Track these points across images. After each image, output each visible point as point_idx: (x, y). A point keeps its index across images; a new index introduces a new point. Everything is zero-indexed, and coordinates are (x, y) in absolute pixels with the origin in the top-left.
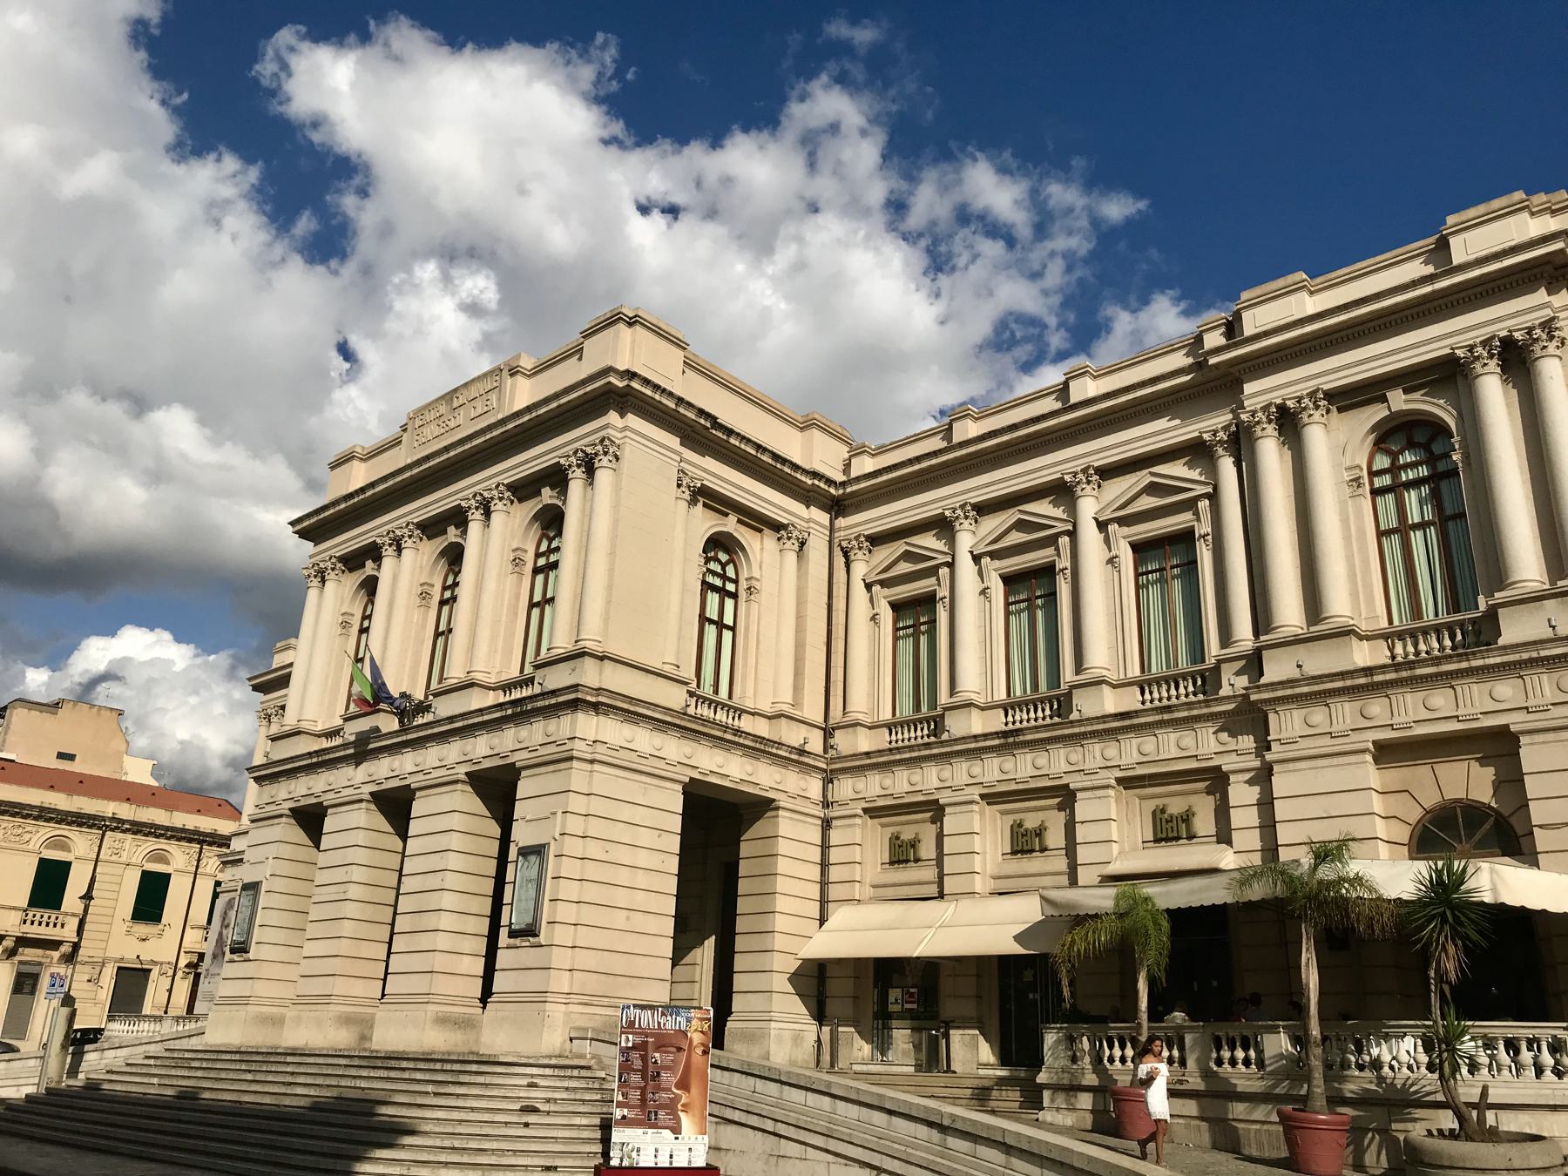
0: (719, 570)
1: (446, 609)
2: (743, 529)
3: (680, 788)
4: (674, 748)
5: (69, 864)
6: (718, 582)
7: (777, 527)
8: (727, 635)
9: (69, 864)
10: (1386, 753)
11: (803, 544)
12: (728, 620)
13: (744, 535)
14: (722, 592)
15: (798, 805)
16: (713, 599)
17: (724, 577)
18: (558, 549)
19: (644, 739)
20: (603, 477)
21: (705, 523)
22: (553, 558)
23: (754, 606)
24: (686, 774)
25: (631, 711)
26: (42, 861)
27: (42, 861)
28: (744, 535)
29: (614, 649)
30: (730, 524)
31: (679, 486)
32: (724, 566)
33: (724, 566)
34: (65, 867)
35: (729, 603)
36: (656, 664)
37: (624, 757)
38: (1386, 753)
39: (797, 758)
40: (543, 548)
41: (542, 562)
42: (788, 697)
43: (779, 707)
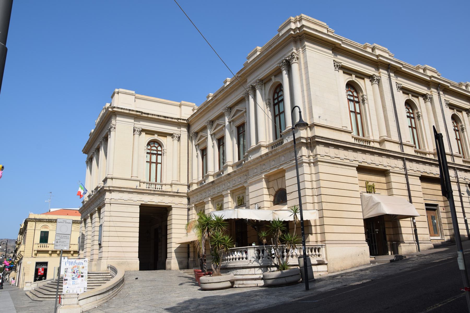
0: (156, 149)
1: (277, 107)
2: (159, 137)
3: (139, 206)
4: (351, 155)
5: (48, 232)
6: (352, 98)
7: (171, 135)
8: (359, 116)
9: (48, 232)
10: (361, 169)
11: (179, 138)
12: (159, 161)
13: (161, 139)
14: (157, 154)
15: (397, 170)
16: (352, 104)
17: (157, 151)
18: (281, 95)
19: (126, 196)
20: (295, 67)
21: (147, 138)
22: (280, 99)
23: (366, 105)
24: (140, 203)
25: (121, 190)
26: (41, 232)
27: (41, 232)
28: (360, 82)
29: (114, 176)
30: (156, 137)
31: (335, 66)
32: (157, 148)
33: (157, 148)
34: (164, 211)
35: (357, 105)
36: (340, 127)
37: (119, 201)
38: (361, 169)
39: (177, 195)
40: (276, 96)
41: (276, 101)
42: (384, 133)
43: (382, 138)
